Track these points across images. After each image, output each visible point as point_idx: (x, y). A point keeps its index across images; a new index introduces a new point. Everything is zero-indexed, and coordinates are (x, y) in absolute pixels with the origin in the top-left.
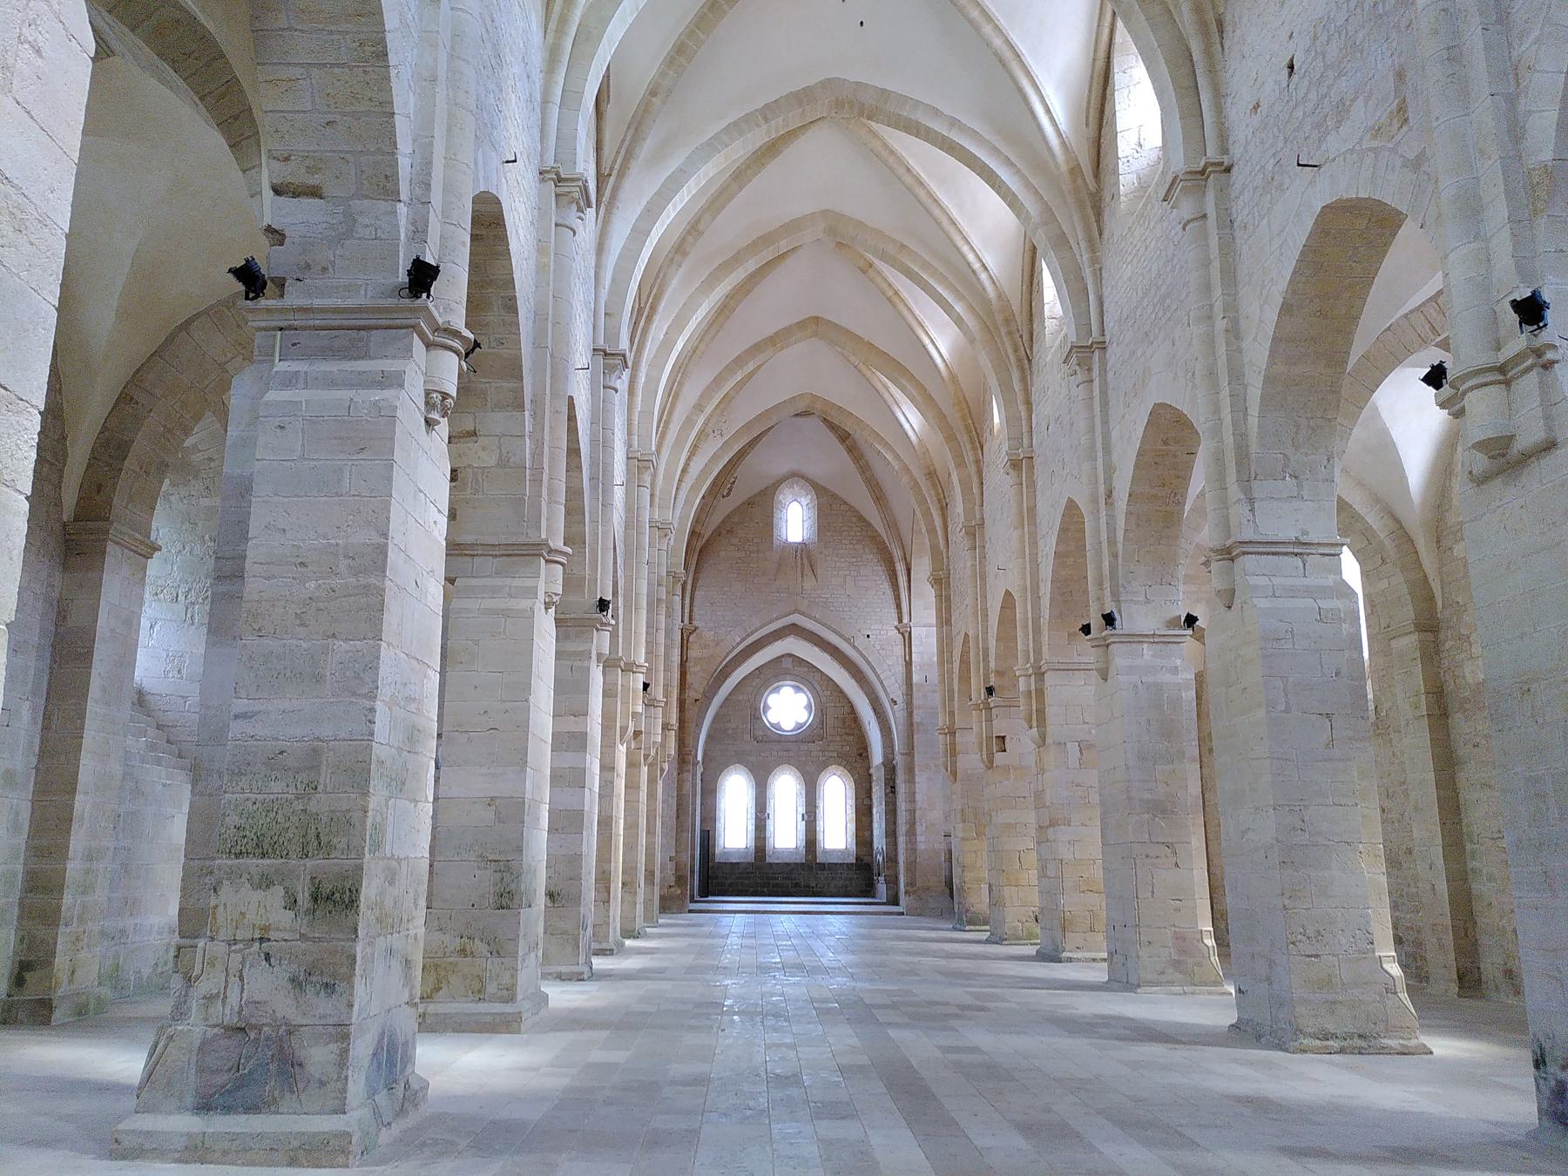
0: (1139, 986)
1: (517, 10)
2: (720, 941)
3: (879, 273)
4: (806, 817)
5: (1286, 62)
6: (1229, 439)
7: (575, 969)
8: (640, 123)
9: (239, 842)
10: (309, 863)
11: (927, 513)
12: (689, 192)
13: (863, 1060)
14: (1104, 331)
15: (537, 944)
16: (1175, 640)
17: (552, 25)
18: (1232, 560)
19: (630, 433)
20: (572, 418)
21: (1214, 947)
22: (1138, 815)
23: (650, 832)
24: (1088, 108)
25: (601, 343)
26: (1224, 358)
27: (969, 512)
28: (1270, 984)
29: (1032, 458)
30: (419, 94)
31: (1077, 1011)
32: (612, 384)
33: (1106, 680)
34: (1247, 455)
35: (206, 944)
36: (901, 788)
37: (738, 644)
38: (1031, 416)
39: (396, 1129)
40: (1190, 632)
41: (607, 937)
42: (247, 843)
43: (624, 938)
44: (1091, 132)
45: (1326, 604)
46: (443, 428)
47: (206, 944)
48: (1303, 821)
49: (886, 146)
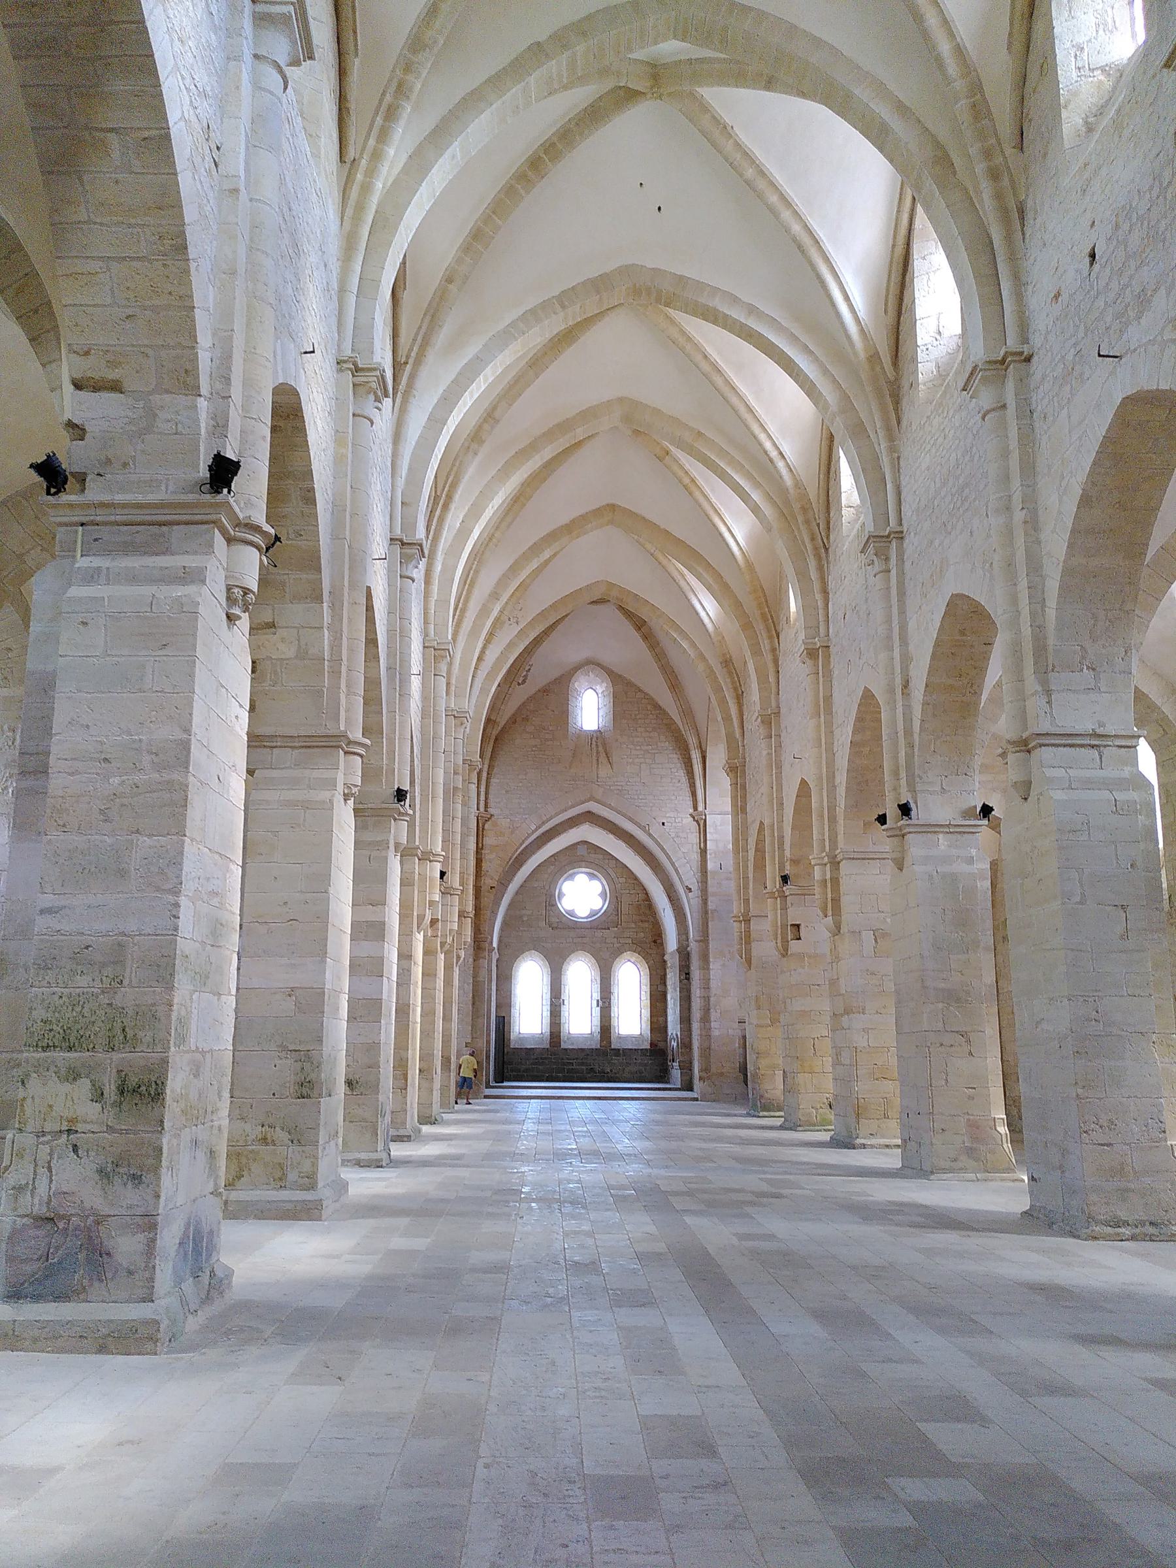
0: (932, 1173)
1: (314, 198)
2: (517, 1127)
3: (676, 461)
4: (600, 1003)
6: (1027, 631)
7: (374, 1156)
8: (437, 310)
9: (46, 1035)
10: (116, 1056)
11: (723, 702)
12: (485, 381)
13: (661, 1247)
14: (901, 520)
15: (337, 1133)
16: (971, 830)
17: (349, 212)
18: (1029, 752)
19: (426, 622)
20: (370, 608)
21: (1006, 1134)
22: (932, 1003)
23: (447, 1018)
24: (887, 296)
25: (398, 532)
26: (1023, 548)
27: (765, 701)
28: (1063, 1172)
29: (829, 647)
31: (871, 1198)
32: (408, 574)
33: (901, 870)
34: (1045, 648)
35: (14, 1136)
36: (696, 974)
37: (534, 832)
38: (828, 604)
39: (202, 1317)
40: (985, 822)
41: (404, 1123)
42: (54, 1036)
43: (420, 1124)
45: (1121, 796)
46: (244, 622)
47: (14, 1136)
49: (683, 332)
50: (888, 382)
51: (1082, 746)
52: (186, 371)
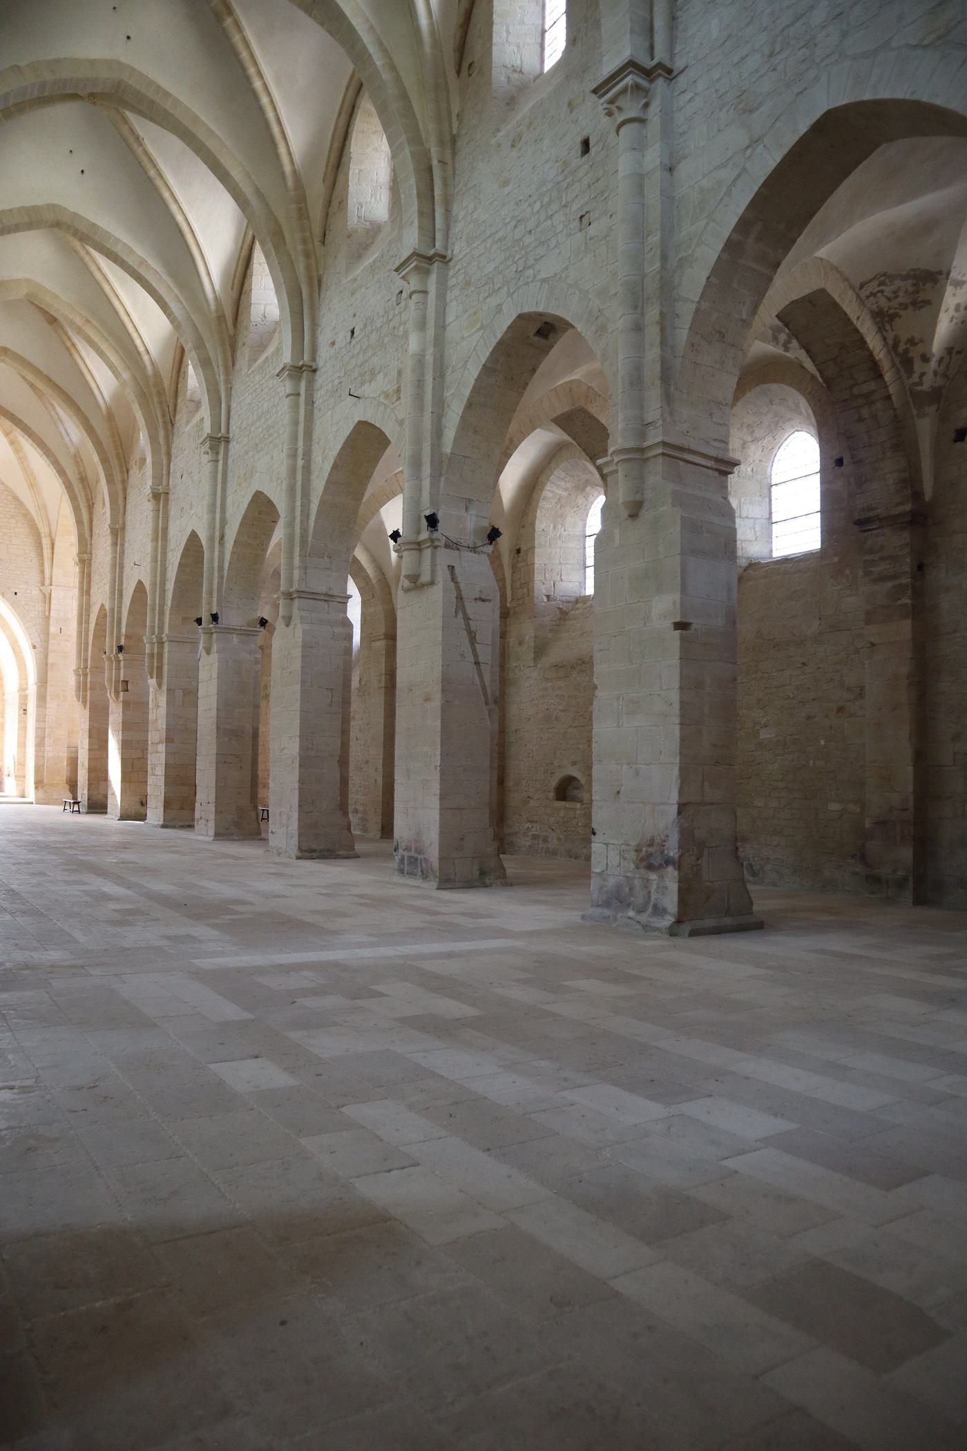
5: (351, 328)
6: (298, 531)
18: (292, 599)
24: (235, 276)
29: (168, 493)
34: (307, 541)
44: (234, 294)
48: (313, 744)
51: (320, 600)
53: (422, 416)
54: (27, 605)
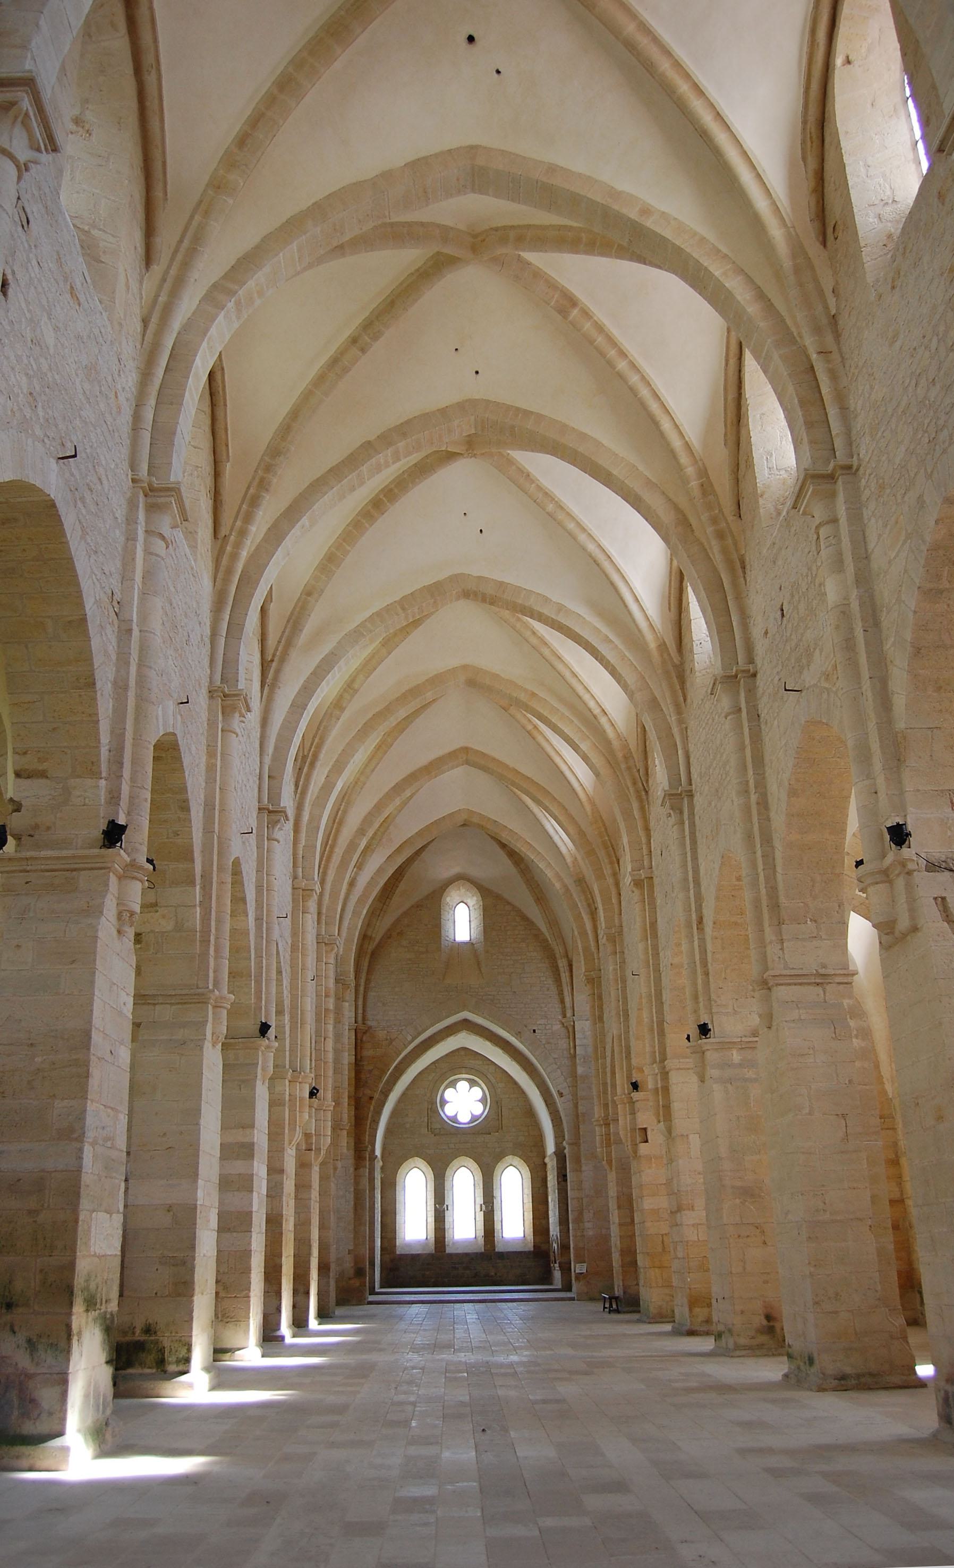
5: (779, 606)
24: (669, 597)
30: (116, 699)
38: (650, 840)
48: (825, 1203)
50: (675, 666)
51: (809, 984)
52: (93, 763)
53: (860, 688)
54: (548, 1043)
